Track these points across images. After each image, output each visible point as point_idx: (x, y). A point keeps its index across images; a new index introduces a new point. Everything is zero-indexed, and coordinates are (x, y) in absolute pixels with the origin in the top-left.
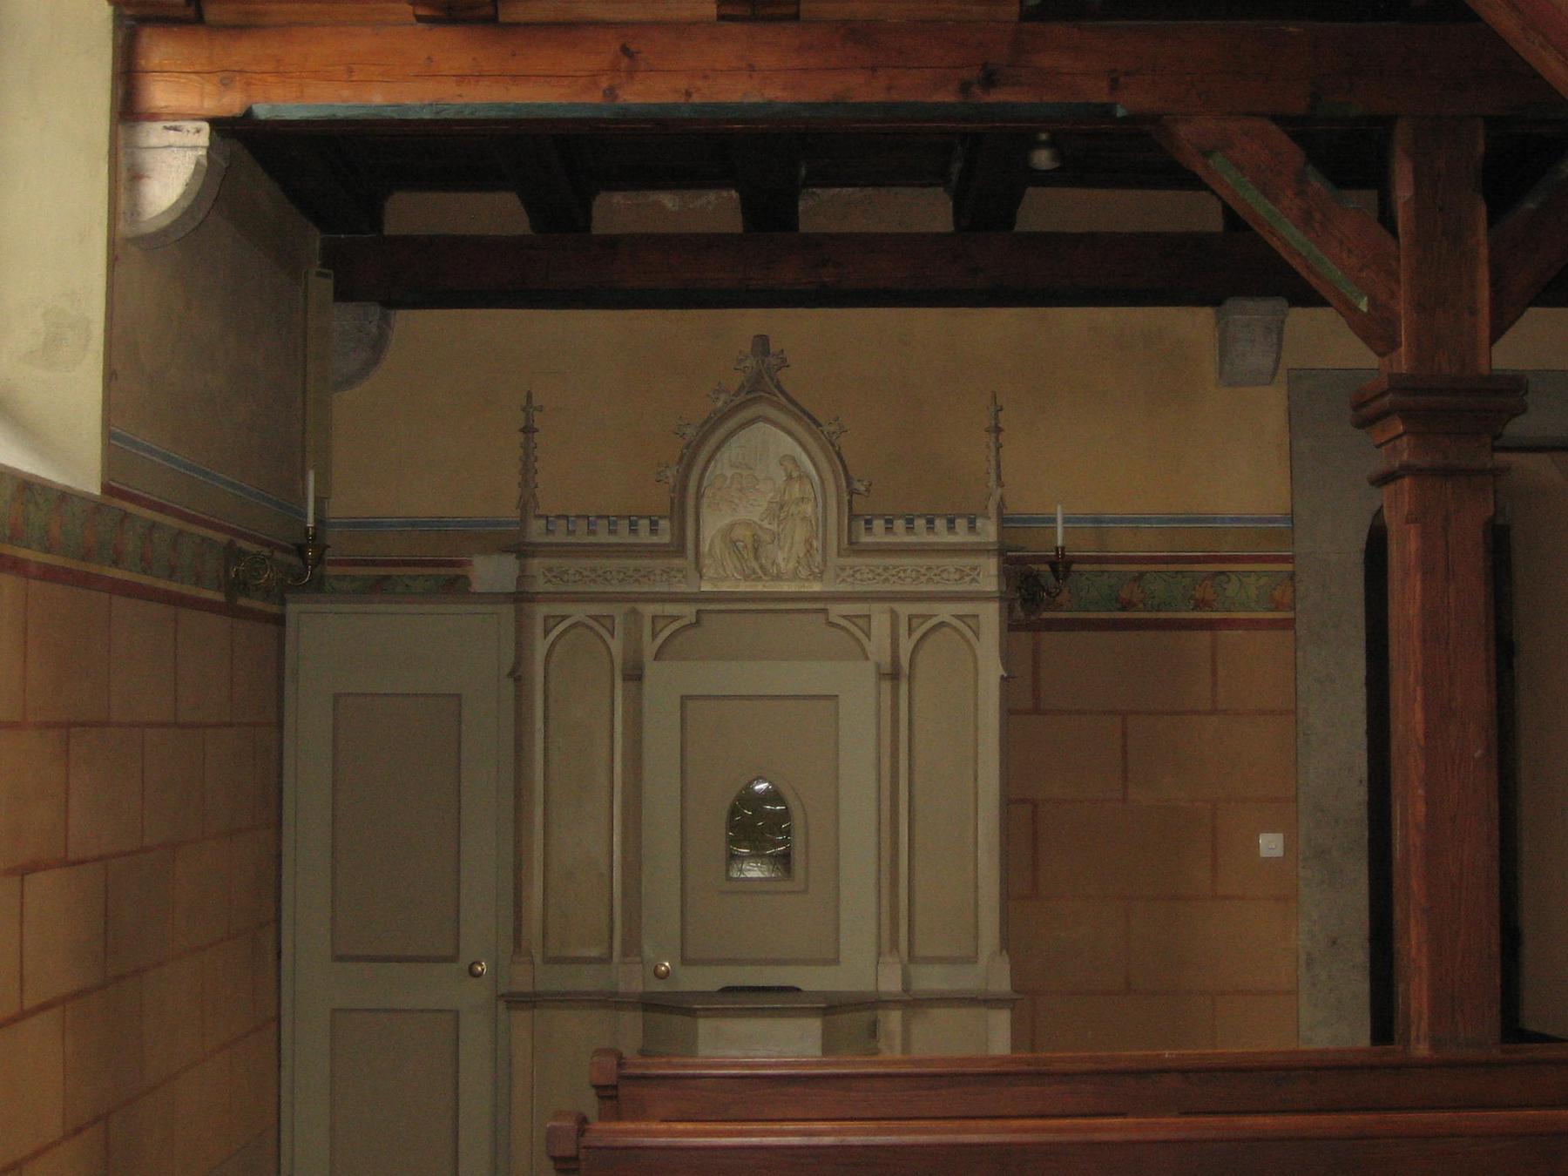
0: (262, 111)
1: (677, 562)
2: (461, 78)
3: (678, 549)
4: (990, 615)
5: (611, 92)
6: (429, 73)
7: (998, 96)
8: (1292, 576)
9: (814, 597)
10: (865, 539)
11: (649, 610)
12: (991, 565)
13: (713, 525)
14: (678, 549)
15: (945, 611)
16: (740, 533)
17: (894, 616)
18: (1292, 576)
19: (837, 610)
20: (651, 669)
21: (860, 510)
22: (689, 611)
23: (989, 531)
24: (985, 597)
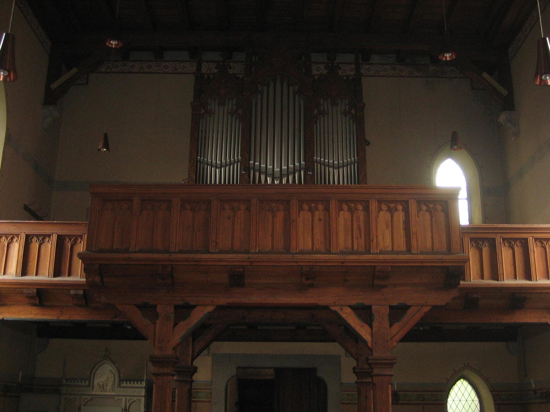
0: (5, 319)
1: (89, 388)
2: (36, 314)
3: (89, 386)
4: (143, 399)
5: (58, 317)
6: (31, 314)
7: (116, 319)
8: (211, 392)
9: (113, 396)
10: (122, 385)
11: (84, 397)
12: (144, 390)
13: (96, 382)
14: (89, 386)
15: (135, 399)
16: (101, 384)
17: (126, 399)
18: (211, 392)
19: (116, 398)
20: (82, 407)
21: (124, 378)
22: (90, 397)
23: (144, 384)
24: (141, 396)
